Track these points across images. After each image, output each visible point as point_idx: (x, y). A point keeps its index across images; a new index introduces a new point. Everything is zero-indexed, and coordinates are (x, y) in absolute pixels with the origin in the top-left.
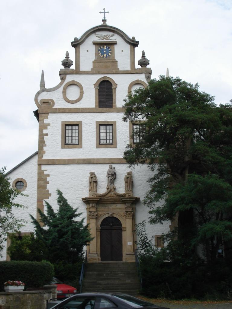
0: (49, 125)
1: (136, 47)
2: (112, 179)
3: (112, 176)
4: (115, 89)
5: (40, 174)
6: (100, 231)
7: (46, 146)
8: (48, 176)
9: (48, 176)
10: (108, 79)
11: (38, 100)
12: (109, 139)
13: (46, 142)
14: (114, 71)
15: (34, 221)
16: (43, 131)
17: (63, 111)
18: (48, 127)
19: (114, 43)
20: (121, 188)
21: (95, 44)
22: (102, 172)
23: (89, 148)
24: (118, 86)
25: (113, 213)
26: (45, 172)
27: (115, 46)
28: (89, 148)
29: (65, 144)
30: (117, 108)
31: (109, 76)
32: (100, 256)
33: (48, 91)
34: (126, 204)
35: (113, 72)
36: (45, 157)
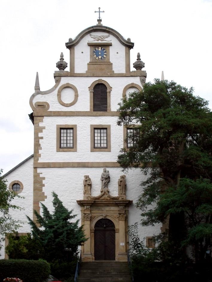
0: (44, 128)
1: (132, 49)
4: (110, 92)
6: (94, 232)
7: (41, 149)
8: (44, 178)
9: (44, 178)
10: (103, 82)
14: (109, 74)
18: (44, 130)
19: (110, 45)
21: (90, 45)
22: (96, 175)
23: (84, 152)
24: (112, 90)
25: (107, 215)
26: (40, 175)
27: (111, 47)
28: (84, 152)
29: (60, 148)
31: (103, 79)
35: (108, 75)
36: (40, 161)
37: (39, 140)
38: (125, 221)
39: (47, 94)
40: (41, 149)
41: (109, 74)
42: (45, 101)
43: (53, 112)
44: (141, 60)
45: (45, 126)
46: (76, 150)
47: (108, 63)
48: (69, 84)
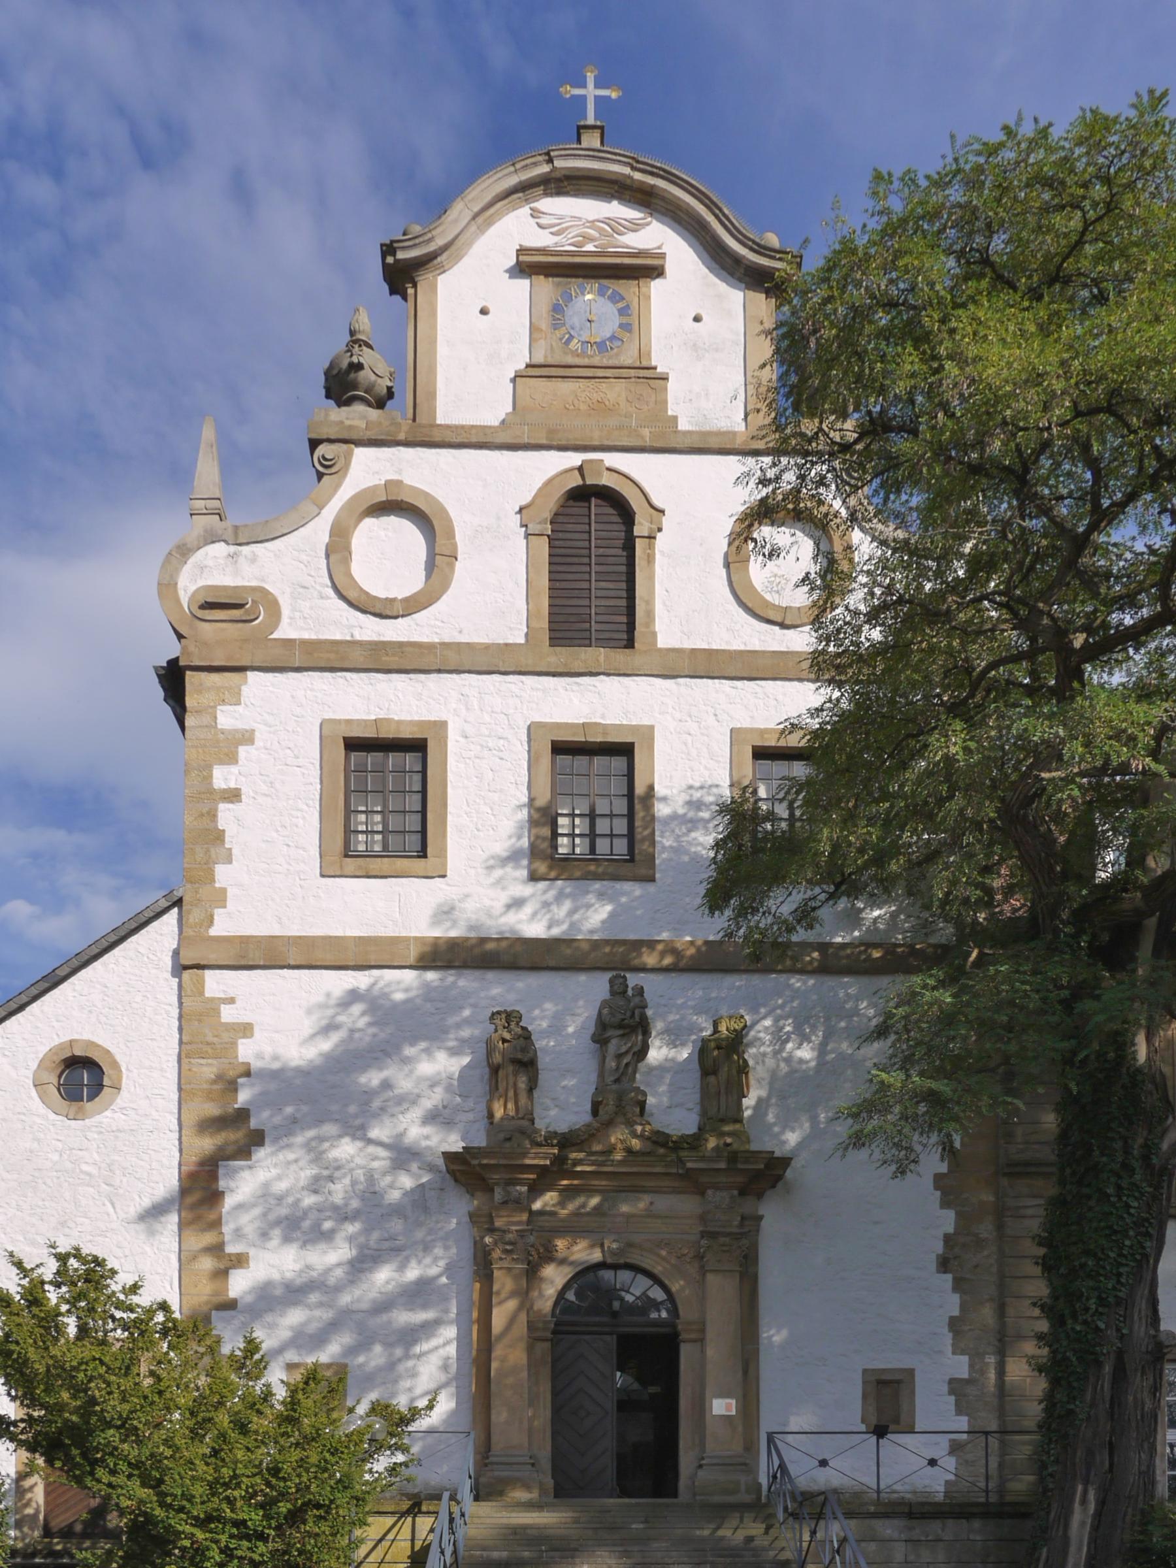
0: (247, 738)
2: (627, 1052)
3: (623, 1025)
4: (652, 537)
5: (200, 1021)
6: (552, 1340)
8: (246, 1030)
10: (606, 480)
11: (181, 593)
12: (612, 836)
13: (227, 839)
14: (646, 432)
15: (174, 1218)
16: (211, 776)
17: (332, 656)
19: (646, 269)
20: (672, 1107)
21: (530, 266)
22: (562, 1016)
24: (666, 522)
25: (630, 1245)
27: (656, 285)
29: (346, 856)
30: (660, 650)
31: (612, 459)
32: (550, 1472)
33: (185, 1061)
34: (710, 1192)
35: (643, 437)
36: (223, 925)
37: (216, 810)
38: (743, 1275)
39: (266, 544)
40: (229, 860)
41: (646, 432)
42: (254, 583)
43: (304, 642)
44: (658, 370)
45: (255, 726)
46: (444, 865)
47: (642, 373)
48: (399, 483)
